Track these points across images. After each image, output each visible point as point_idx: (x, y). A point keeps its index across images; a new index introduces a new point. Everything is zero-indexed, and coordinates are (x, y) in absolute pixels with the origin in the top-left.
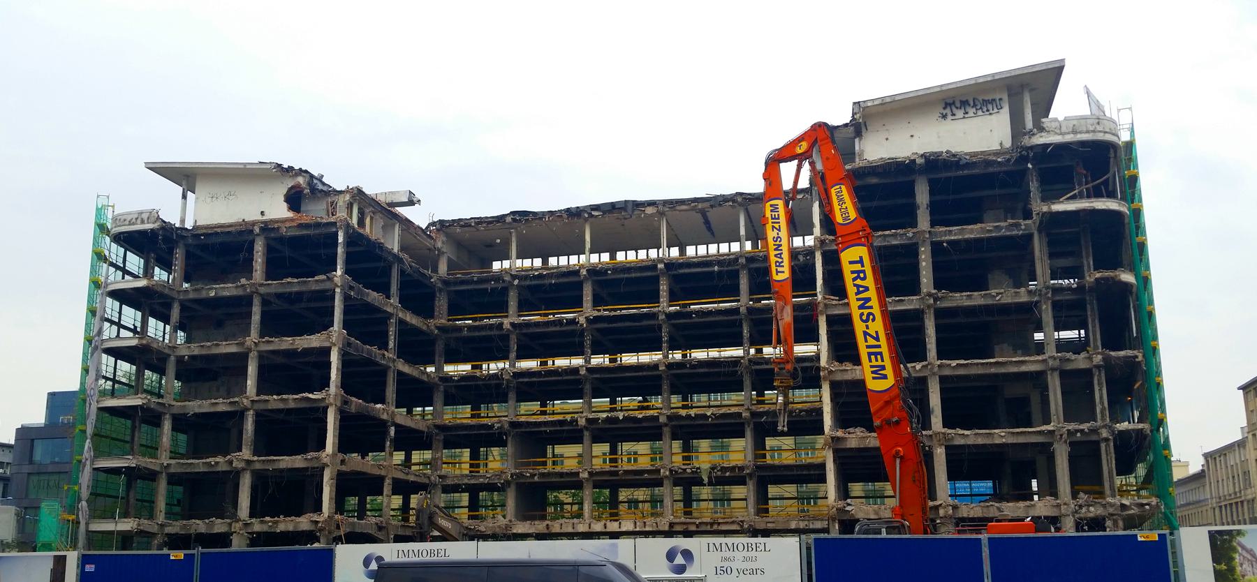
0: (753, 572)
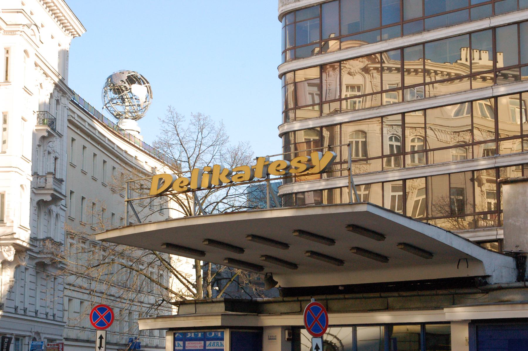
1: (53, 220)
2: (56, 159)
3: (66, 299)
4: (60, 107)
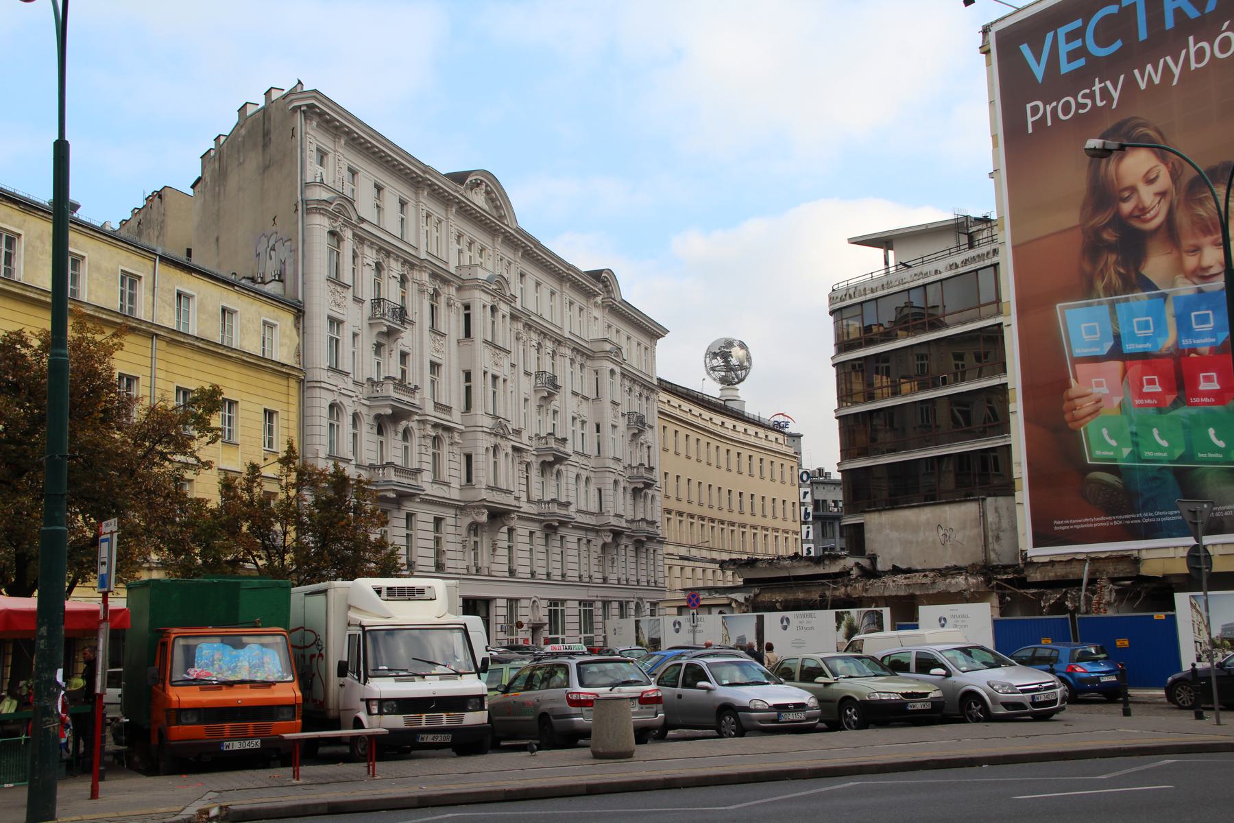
0: (965, 626)
1: (649, 501)
2: (649, 447)
3: (667, 567)
4: (585, 370)
